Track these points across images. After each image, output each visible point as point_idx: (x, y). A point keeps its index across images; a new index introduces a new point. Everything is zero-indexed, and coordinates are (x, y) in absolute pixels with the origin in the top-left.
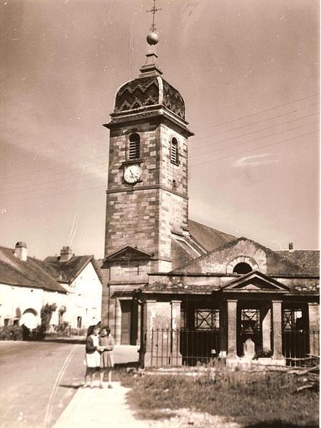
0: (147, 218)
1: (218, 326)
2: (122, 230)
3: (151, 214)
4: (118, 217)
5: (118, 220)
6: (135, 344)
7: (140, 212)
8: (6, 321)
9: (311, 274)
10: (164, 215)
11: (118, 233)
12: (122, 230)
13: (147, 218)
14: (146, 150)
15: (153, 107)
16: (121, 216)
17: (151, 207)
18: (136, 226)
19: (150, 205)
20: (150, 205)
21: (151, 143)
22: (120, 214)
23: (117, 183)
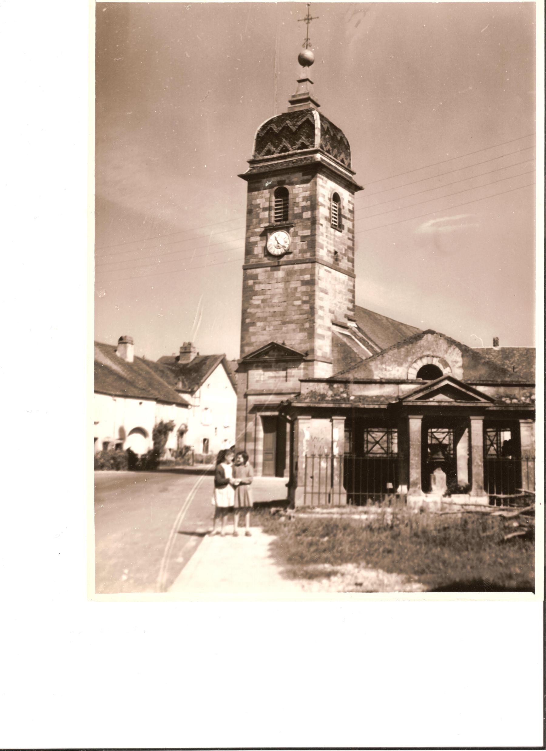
0: (298, 303)
2: (265, 319)
5: (258, 306)
7: (289, 295)
12: (265, 319)
13: (298, 303)
14: (297, 210)
16: (263, 301)
17: (304, 288)
18: (283, 314)
22: (262, 297)
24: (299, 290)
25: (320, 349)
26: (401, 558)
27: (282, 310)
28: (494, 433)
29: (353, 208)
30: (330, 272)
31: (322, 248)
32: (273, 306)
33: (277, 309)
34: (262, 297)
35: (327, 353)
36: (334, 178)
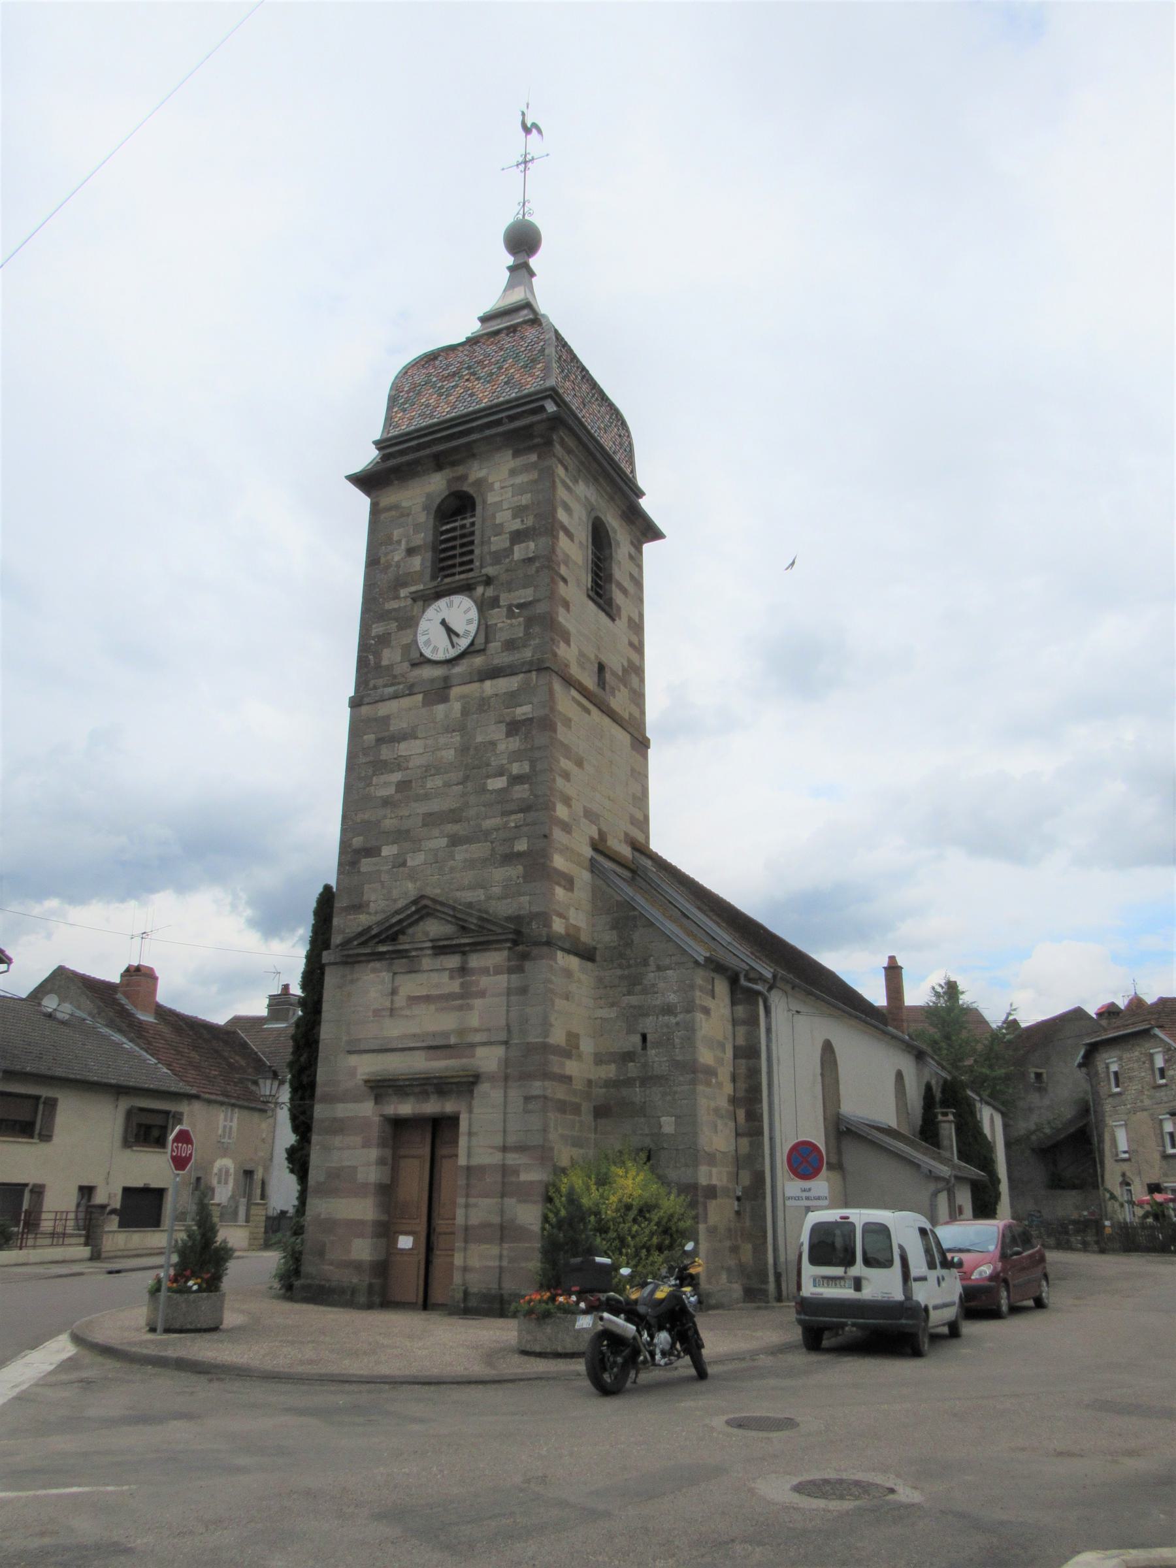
0: (499, 783)
1: (598, 1259)
2: (400, 835)
3: (515, 769)
4: (391, 791)
5: (386, 802)
6: (181, 1114)
7: (474, 763)
8: (86, 1191)
9: (431, 1052)
10: (566, 776)
11: (386, 851)
12: (400, 835)
13: (499, 783)
14: (499, 543)
15: (512, 418)
16: (403, 786)
17: (515, 743)
18: (454, 816)
19: (509, 734)
20: (509, 734)
21: (515, 517)
22: (396, 777)
23: (390, 667)
24: (501, 747)
25: (561, 916)
26: (671, 1236)
27: (454, 806)
28: (502, 980)
29: (600, 832)
30: (588, 712)
31: (568, 642)
32: (426, 797)
33: (435, 806)
34: (396, 777)
35: (578, 929)
36: (596, 480)
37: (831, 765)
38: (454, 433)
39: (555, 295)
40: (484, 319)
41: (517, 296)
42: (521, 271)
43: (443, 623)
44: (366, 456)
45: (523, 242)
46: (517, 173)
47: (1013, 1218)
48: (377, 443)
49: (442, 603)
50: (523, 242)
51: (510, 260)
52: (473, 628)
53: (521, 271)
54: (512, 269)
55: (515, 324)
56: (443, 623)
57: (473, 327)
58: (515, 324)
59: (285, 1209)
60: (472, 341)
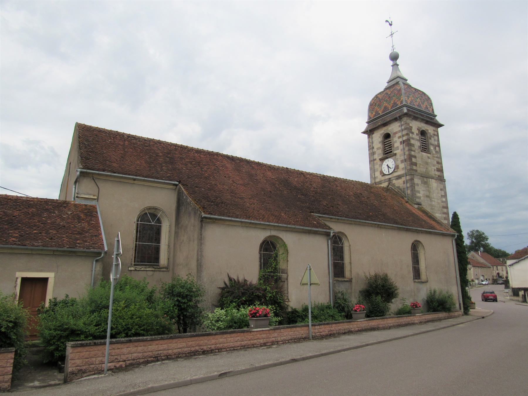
37: (471, 184)
38: (432, 232)
39: (404, 71)
40: (388, 83)
41: (395, 75)
42: (395, 66)
43: (387, 165)
44: (364, 126)
45: (394, 57)
46: (390, 37)
47: (55, 303)
48: (367, 123)
49: (387, 160)
50: (394, 57)
51: (391, 63)
52: (394, 166)
53: (395, 66)
54: (392, 66)
55: (397, 84)
56: (387, 165)
57: (386, 85)
58: (397, 84)
59: (489, 240)
60: (386, 89)
